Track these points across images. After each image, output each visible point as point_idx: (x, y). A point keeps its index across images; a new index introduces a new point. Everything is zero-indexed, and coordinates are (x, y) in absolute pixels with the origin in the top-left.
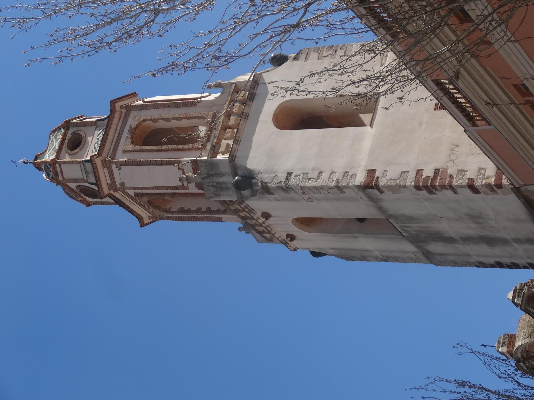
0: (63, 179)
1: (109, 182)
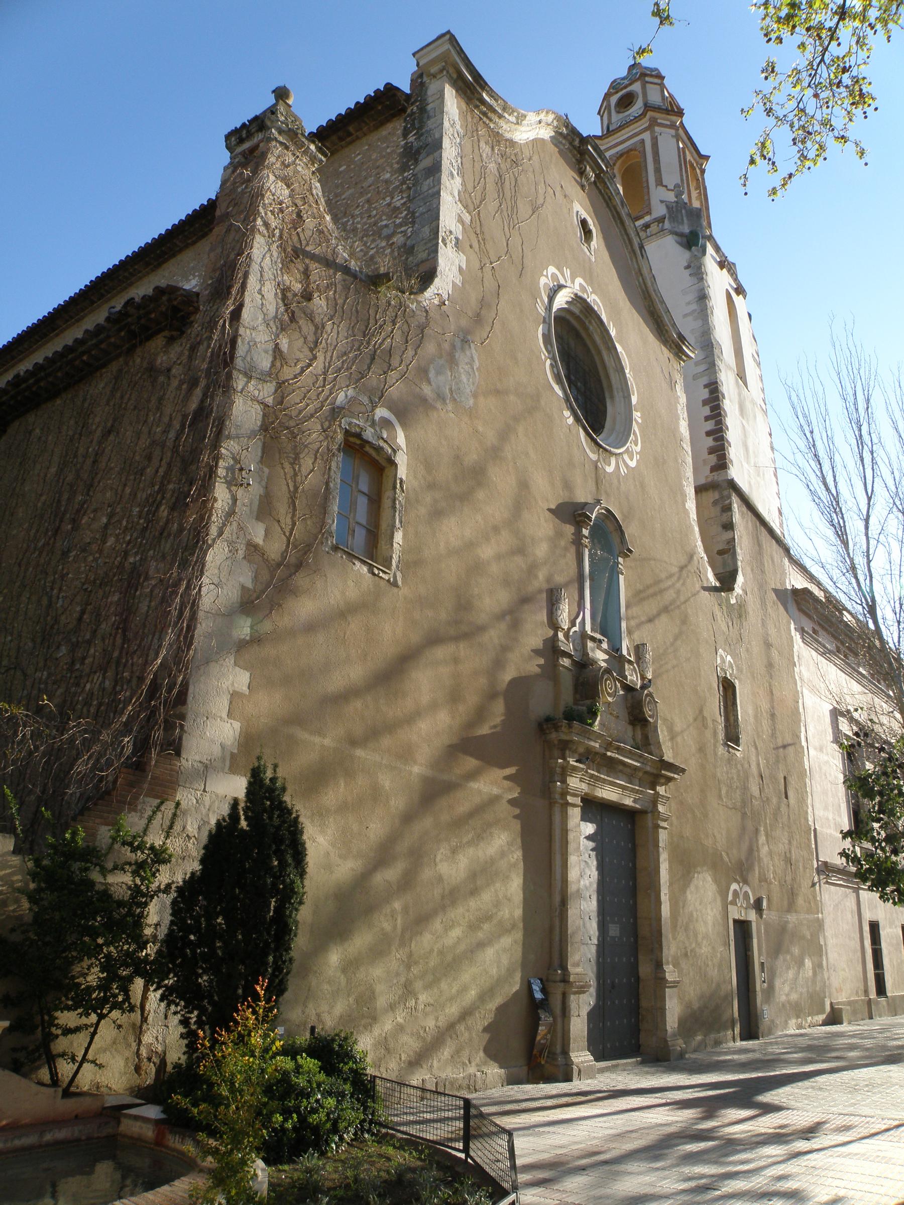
0: (647, 82)
1: (659, 121)
